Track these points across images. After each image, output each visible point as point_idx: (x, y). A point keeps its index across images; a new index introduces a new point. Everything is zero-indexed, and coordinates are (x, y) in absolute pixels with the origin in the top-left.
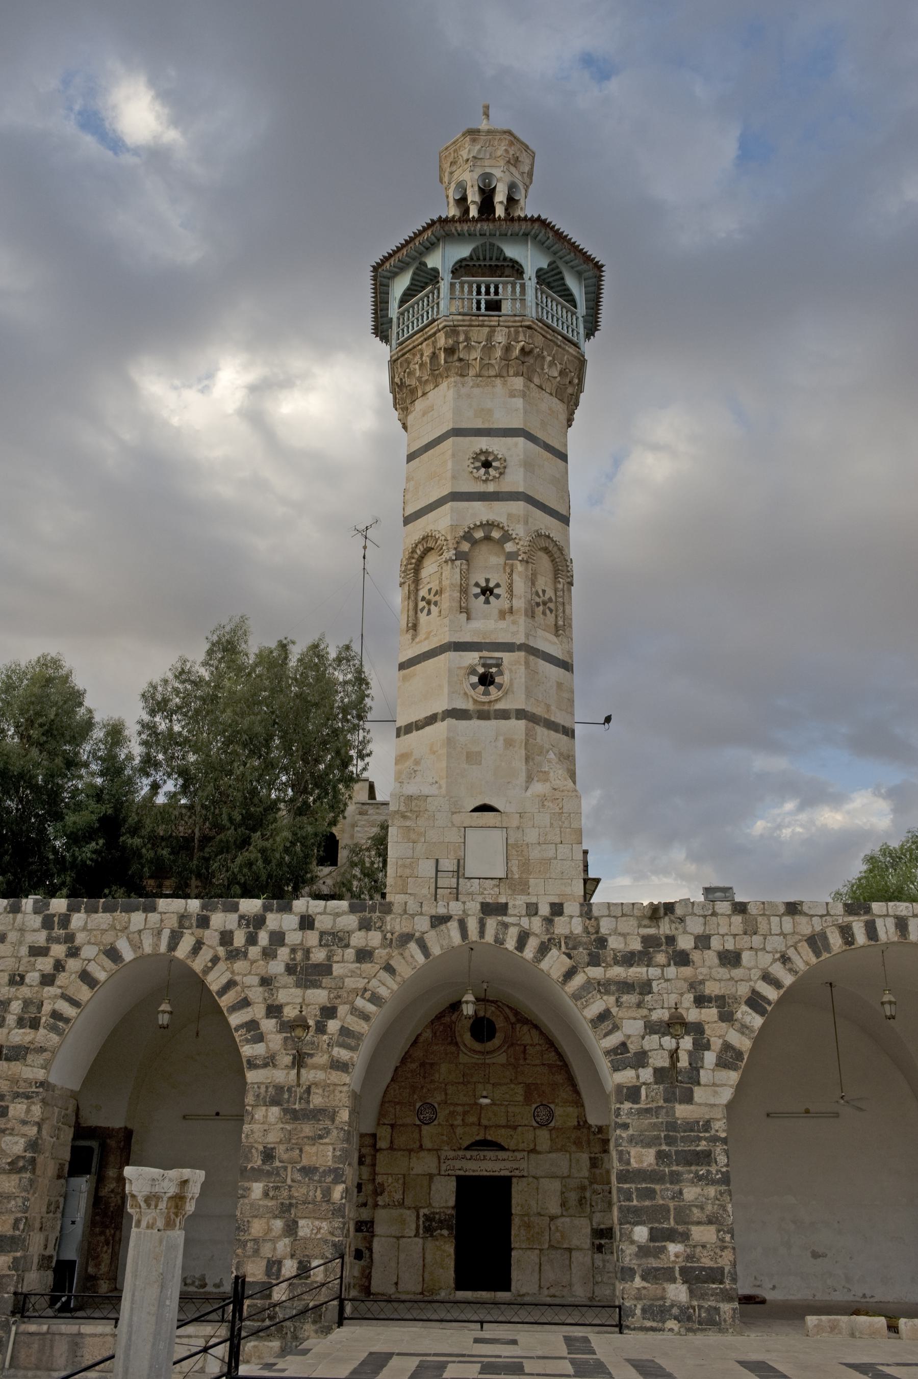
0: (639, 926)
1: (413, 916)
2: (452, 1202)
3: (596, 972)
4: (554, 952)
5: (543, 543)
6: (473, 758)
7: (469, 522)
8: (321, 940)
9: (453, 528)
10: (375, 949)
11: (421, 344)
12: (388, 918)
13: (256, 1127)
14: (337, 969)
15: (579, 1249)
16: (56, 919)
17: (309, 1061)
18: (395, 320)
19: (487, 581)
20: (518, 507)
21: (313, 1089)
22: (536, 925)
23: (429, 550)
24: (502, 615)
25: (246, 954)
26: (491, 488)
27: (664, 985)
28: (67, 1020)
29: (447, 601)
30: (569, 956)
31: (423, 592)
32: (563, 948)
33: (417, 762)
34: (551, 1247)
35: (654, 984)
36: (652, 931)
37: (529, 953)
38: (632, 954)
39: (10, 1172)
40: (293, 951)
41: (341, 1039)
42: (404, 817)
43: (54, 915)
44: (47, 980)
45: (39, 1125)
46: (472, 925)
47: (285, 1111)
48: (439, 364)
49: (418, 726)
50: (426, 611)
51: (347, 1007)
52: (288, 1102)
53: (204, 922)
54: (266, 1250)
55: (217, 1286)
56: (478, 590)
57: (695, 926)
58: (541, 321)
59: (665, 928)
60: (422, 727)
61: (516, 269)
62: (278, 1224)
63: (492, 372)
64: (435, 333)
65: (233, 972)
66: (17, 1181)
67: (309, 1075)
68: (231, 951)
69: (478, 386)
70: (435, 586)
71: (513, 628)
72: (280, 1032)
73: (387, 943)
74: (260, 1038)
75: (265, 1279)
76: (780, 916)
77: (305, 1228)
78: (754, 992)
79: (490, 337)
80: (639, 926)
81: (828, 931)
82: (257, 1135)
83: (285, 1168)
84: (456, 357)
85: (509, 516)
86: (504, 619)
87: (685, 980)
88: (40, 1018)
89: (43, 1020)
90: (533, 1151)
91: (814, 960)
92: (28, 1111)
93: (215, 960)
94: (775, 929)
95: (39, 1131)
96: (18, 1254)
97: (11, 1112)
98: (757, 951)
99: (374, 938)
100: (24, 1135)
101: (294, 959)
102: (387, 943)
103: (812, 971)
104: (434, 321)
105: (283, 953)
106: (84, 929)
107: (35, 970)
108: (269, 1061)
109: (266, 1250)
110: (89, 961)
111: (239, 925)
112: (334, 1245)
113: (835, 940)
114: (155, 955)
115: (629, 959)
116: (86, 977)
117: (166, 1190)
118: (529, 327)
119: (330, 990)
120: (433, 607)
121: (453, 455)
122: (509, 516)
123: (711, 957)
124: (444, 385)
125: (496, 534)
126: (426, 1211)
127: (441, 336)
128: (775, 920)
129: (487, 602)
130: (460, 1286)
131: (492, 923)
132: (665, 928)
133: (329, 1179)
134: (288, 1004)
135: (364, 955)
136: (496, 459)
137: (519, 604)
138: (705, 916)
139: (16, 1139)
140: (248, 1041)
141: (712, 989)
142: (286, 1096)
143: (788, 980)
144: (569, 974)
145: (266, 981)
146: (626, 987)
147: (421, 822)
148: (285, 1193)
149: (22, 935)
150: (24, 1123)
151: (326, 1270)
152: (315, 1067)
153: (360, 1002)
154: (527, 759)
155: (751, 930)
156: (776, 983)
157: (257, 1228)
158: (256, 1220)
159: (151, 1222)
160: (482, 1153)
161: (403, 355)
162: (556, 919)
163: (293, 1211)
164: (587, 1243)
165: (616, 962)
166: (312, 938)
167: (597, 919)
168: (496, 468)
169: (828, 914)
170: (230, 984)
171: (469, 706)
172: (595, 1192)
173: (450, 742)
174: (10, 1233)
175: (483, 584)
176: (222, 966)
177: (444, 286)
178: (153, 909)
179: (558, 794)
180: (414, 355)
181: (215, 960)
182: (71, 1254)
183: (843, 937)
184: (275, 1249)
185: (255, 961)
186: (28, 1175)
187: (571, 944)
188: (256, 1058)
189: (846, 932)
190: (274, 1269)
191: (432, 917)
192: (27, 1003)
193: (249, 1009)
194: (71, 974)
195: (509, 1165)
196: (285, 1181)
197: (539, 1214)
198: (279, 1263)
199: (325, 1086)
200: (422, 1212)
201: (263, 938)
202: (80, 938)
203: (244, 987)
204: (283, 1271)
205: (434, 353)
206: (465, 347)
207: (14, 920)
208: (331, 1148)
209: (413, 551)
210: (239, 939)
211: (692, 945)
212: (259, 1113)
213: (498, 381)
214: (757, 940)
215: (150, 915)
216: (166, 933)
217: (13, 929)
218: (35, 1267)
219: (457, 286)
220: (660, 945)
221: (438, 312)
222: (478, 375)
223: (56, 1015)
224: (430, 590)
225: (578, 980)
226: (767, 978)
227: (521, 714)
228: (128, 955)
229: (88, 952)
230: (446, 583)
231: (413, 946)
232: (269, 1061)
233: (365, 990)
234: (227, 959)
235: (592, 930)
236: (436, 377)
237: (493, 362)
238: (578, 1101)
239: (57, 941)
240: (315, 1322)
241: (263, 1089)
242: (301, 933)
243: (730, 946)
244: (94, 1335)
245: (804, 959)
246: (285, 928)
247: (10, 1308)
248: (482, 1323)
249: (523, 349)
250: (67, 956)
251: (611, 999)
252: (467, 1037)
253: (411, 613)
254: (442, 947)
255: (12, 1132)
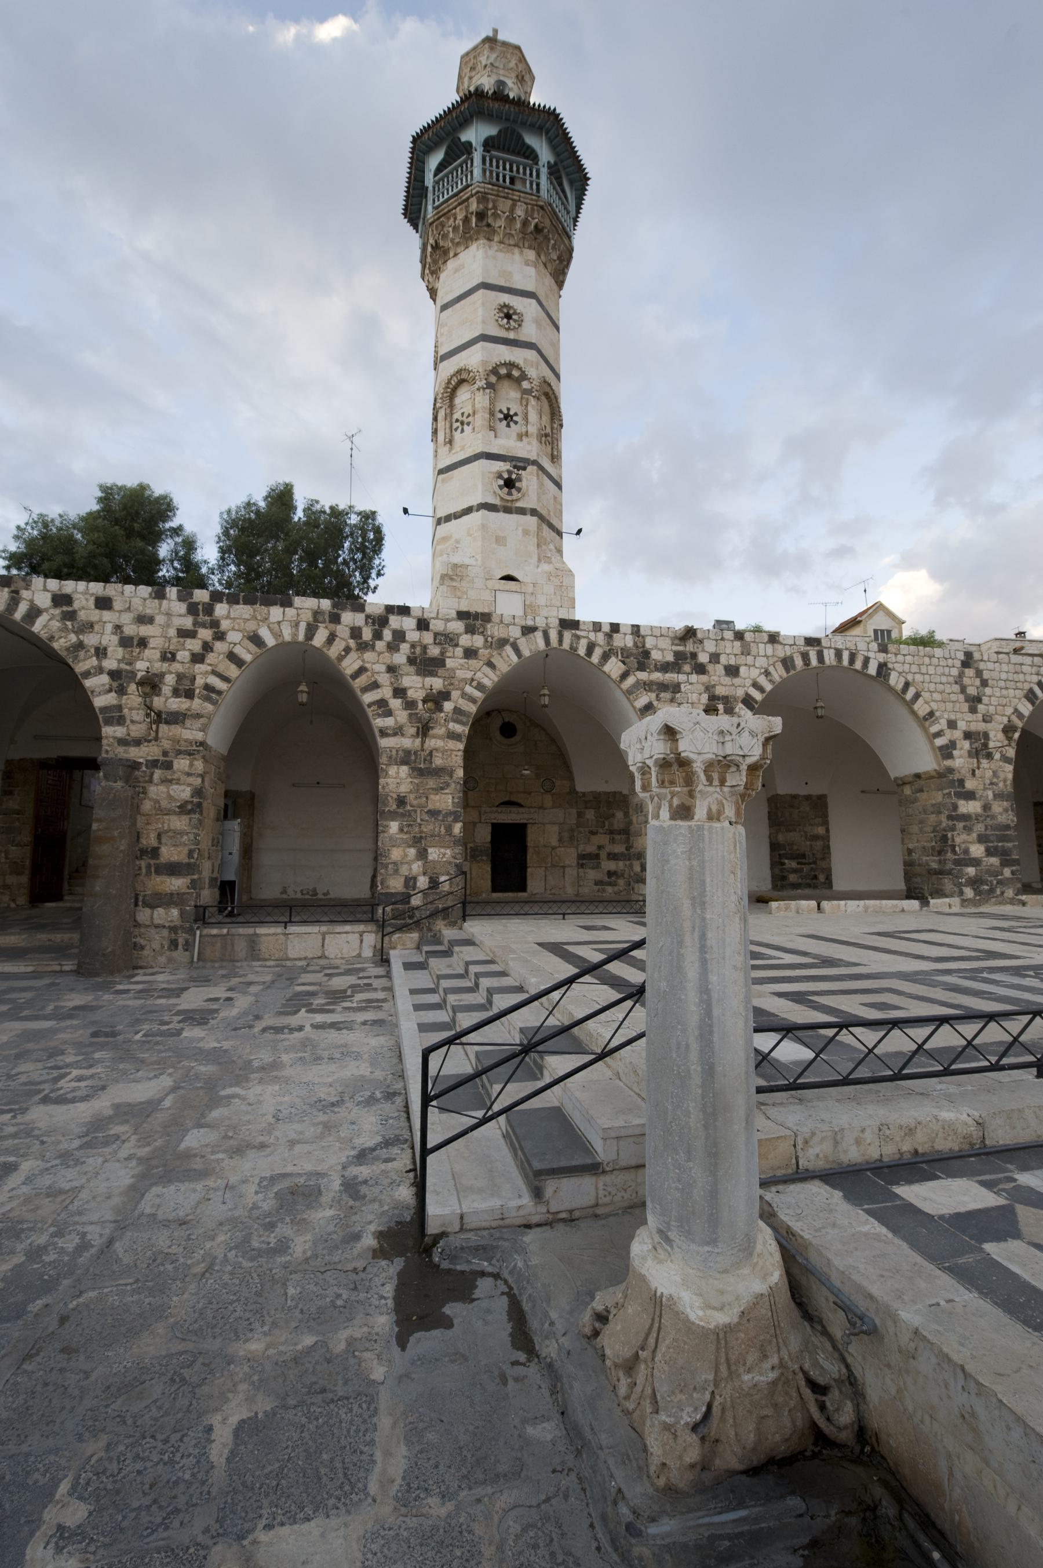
0: (673, 644)
1: (508, 625)
2: (489, 839)
3: (643, 676)
4: (613, 659)
5: (548, 390)
6: (500, 540)
7: (496, 360)
8: (435, 639)
9: (484, 363)
10: (479, 649)
11: (455, 208)
12: (489, 626)
13: (390, 781)
14: (450, 663)
15: (569, 866)
16: (200, 607)
17: (431, 732)
18: (430, 189)
19: (508, 409)
20: (531, 355)
21: (435, 753)
22: (600, 638)
23: (462, 382)
24: (520, 437)
25: (373, 647)
26: (511, 335)
27: (689, 687)
28: (219, 693)
29: (480, 420)
30: (624, 663)
31: (455, 416)
32: (620, 657)
33: (458, 542)
34: (553, 866)
35: (682, 686)
36: (681, 648)
37: (595, 659)
38: (668, 663)
39: (180, 813)
40: (413, 646)
41: (455, 716)
42: (452, 579)
43: (198, 604)
44: (197, 658)
45: (202, 776)
46: (553, 635)
47: (413, 769)
48: (471, 228)
49: (457, 516)
50: (459, 430)
51: (459, 692)
52: (415, 762)
53: (335, 619)
54: (404, 870)
55: (324, 894)
56: (502, 416)
57: (710, 646)
58: (550, 205)
59: (690, 647)
60: (460, 517)
61: (531, 155)
62: (412, 852)
63: (512, 242)
64: (468, 199)
65: (363, 661)
66: (188, 821)
67: (431, 743)
68: (361, 644)
69: (501, 251)
70: (468, 410)
71: (529, 448)
72: (405, 709)
73: (488, 645)
74: (389, 713)
75: (404, 890)
76: (765, 643)
77: (433, 854)
78: (747, 694)
79: (512, 210)
80: (673, 644)
81: (795, 655)
82: (392, 787)
83: (415, 811)
84: (484, 223)
85: (525, 360)
86: (521, 440)
87: (703, 684)
88: (194, 690)
89: (197, 691)
90: (541, 807)
91: (785, 675)
92: (191, 765)
93: (347, 650)
94: (762, 653)
95: (203, 781)
96: (195, 877)
97: (176, 766)
98: (749, 666)
99: (478, 641)
100: (189, 785)
101: (414, 653)
102: (488, 645)
103: (784, 681)
104: (468, 186)
105: (405, 648)
106: (228, 617)
107: (184, 649)
108: (398, 731)
109: (404, 870)
110: (235, 644)
111: (367, 623)
112: (456, 865)
113: (799, 662)
114: (294, 643)
115: (665, 668)
116: (232, 657)
117: (746, 752)
118: (542, 207)
119: (445, 678)
120: (465, 427)
121: (483, 304)
122: (525, 360)
123: (720, 669)
124: (473, 247)
125: (516, 373)
126: (472, 845)
127: (473, 201)
128: (761, 646)
129: (508, 426)
130: (494, 889)
131: (567, 635)
132: (690, 647)
133: (450, 819)
134: (411, 688)
135: (470, 653)
136: (515, 313)
137: (533, 429)
138: (716, 640)
139: (183, 787)
140: (379, 715)
141: (720, 691)
142: (413, 758)
143: (769, 687)
144: (624, 676)
145: (391, 669)
146: (663, 687)
147: (464, 583)
148: (417, 829)
149: (169, 619)
150: (189, 774)
151: (451, 884)
152: (434, 737)
153: (468, 689)
154: (539, 546)
155: (746, 651)
156: (761, 690)
157: (396, 854)
158: (395, 849)
159: (714, 808)
160: (508, 810)
161: (439, 218)
162: (615, 635)
163: (423, 842)
164: (574, 862)
165: (657, 669)
166: (428, 638)
167: (643, 637)
168: (515, 321)
169: (795, 644)
170: (362, 670)
171: (496, 501)
172: (580, 832)
173: (484, 527)
174: (187, 860)
175: (506, 412)
176: (353, 655)
177: (477, 157)
178: (290, 604)
179: (559, 573)
180: (449, 219)
181: (347, 650)
182: (231, 876)
183: (804, 660)
184: (411, 869)
185: (382, 653)
186: (197, 816)
187: (625, 654)
188: (387, 728)
189: (805, 656)
190: (411, 884)
191: (522, 627)
192: (180, 677)
193: (379, 690)
194: (219, 654)
195: (526, 816)
196: (415, 821)
197: (545, 846)
198: (415, 879)
199: (444, 751)
200: (469, 846)
201: (387, 635)
202: (225, 625)
203: (373, 673)
204: (418, 884)
205: (466, 217)
206: (493, 214)
207: (160, 605)
208: (450, 797)
209: (449, 382)
210: (367, 634)
211: (708, 660)
212: (392, 770)
213: (516, 250)
214: (750, 659)
215: (287, 609)
216: (303, 626)
217: (160, 612)
218: (207, 886)
219: (488, 159)
220: (686, 659)
221: (472, 179)
222: (501, 242)
223: (208, 687)
224: (463, 414)
225: (630, 680)
226: (756, 685)
227: (534, 512)
228: (270, 641)
229: (233, 637)
230: (478, 406)
231: (508, 649)
232: (398, 731)
233: (473, 680)
234: (357, 650)
235: (640, 645)
236: (467, 238)
237: (513, 232)
238: (570, 777)
239: (204, 625)
240: (444, 919)
241: (394, 752)
242: (418, 633)
243: (732, 662)
244: (266, 935)
245: (779, 673)
246: (405, 628)
247: (193, 918)
248: (564, 914)
249: (536, 226)
250: (213, 639)
251: (653, 695)
252: (498, 734)
253: (448, 431)
254: (531, 650)
255: (178, 782)
